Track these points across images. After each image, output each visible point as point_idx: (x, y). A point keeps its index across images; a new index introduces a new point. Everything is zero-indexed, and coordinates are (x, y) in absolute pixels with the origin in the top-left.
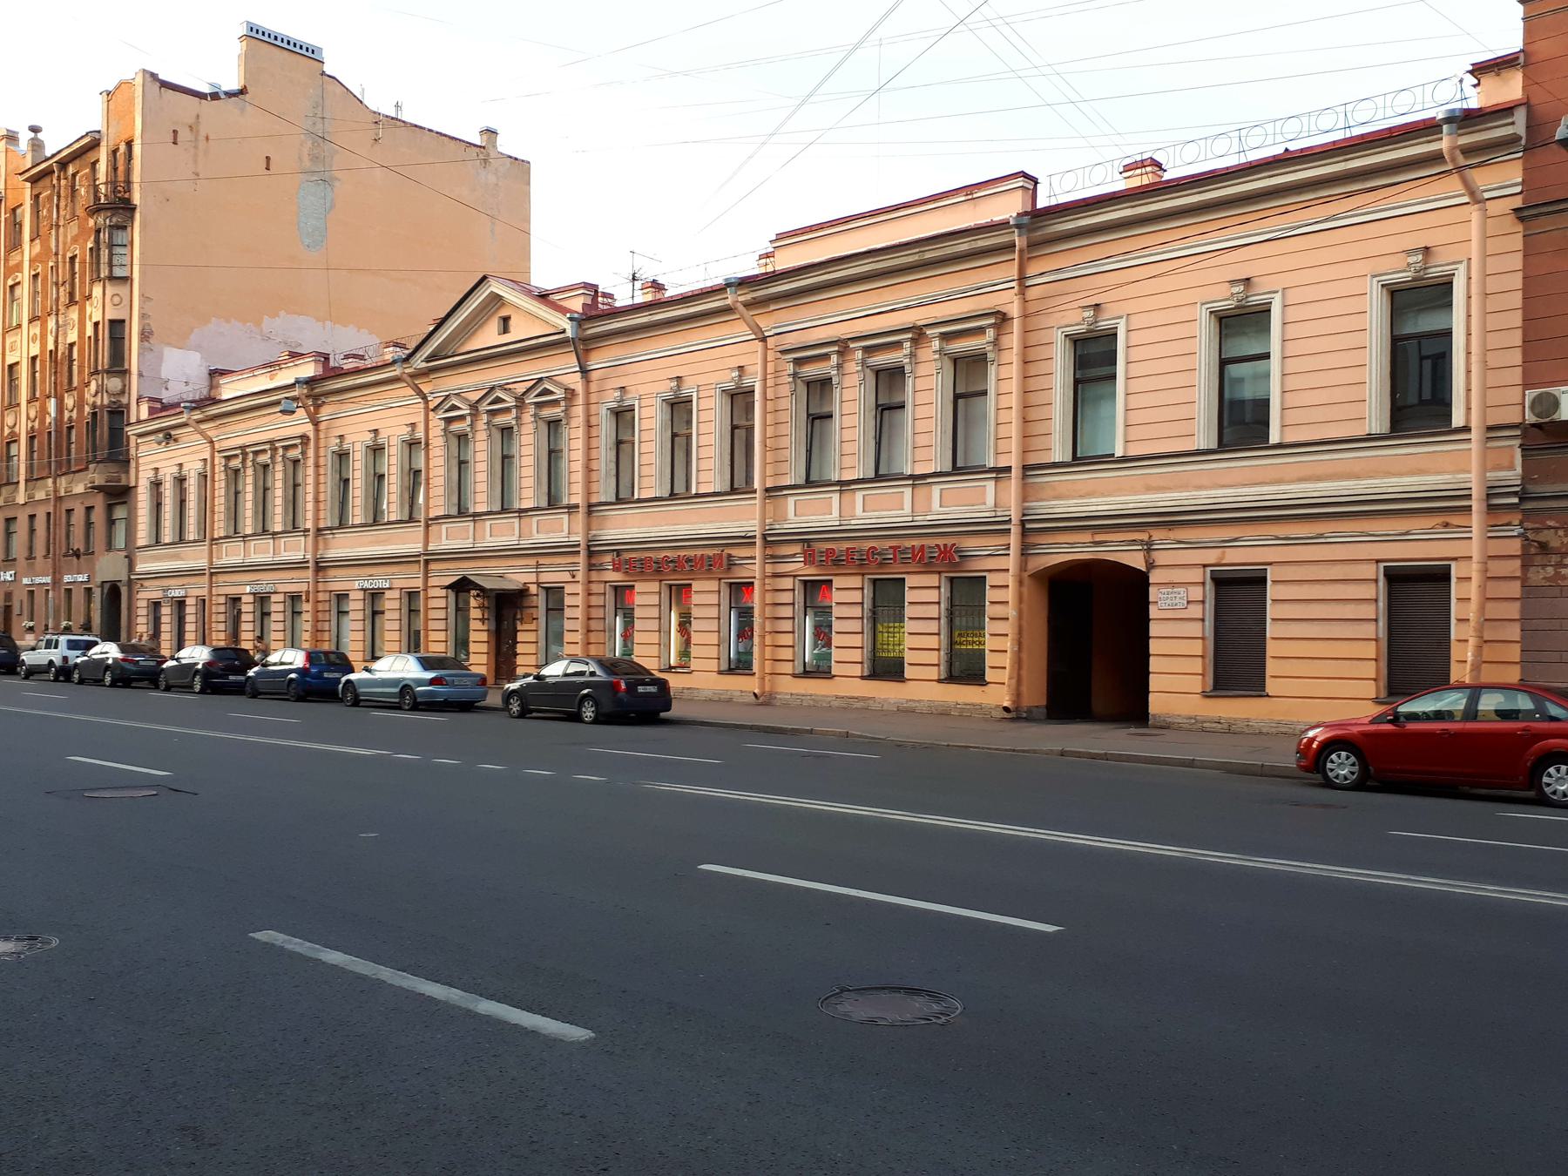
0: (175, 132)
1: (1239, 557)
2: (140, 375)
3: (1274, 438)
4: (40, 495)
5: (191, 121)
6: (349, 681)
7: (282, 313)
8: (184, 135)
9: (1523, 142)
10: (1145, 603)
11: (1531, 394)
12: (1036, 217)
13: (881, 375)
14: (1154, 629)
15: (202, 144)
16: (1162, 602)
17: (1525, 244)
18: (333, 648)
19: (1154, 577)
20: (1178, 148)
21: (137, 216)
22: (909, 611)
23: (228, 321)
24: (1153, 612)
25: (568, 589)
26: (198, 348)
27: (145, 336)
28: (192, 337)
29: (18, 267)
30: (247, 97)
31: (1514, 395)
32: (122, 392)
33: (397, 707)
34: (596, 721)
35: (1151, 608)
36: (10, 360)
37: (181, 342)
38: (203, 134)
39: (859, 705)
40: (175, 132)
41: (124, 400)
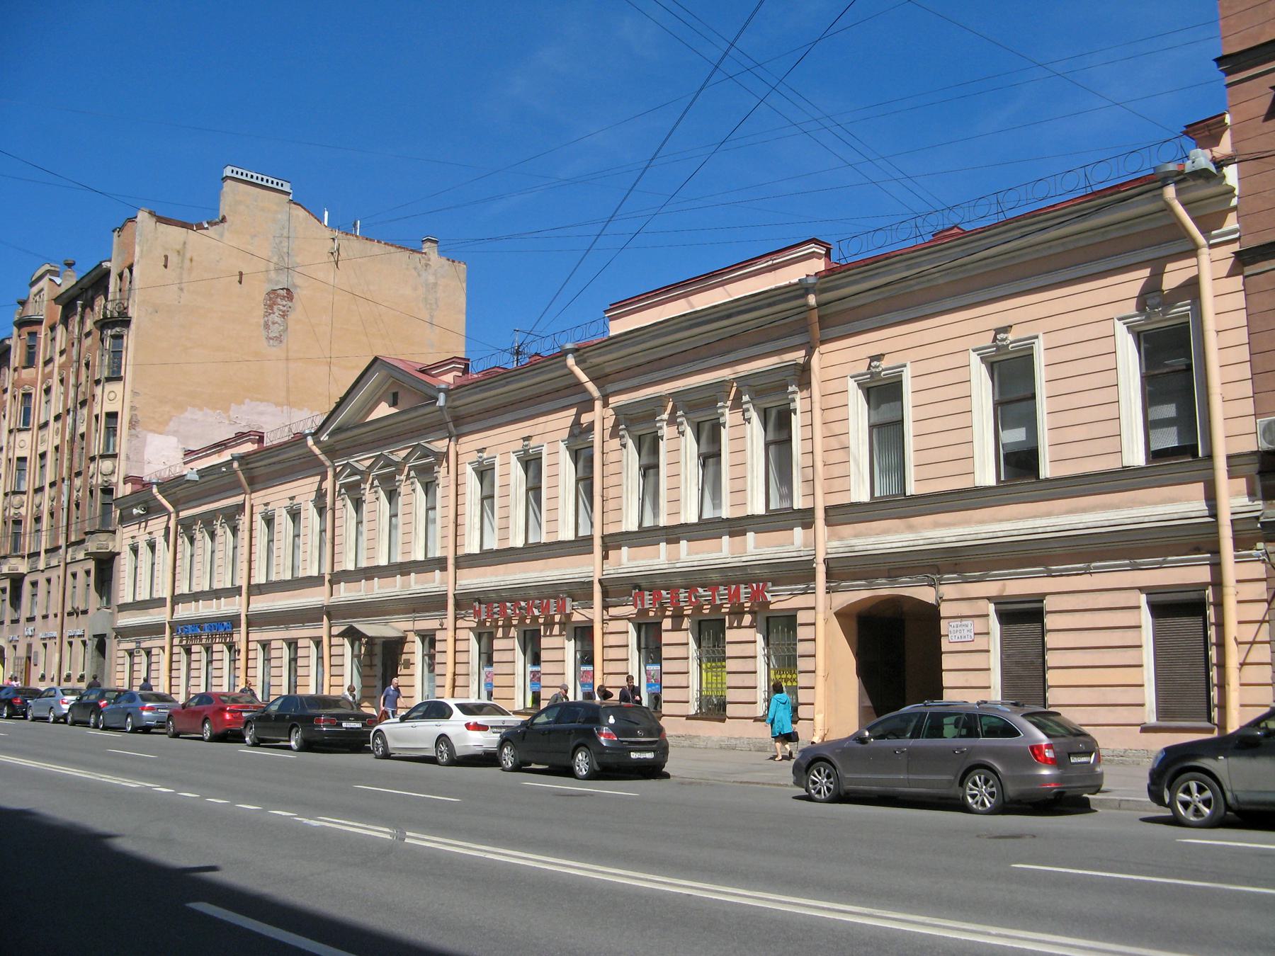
0: (166, 257)
1: (1020, 586)
2: (128, 458)
3: (1046, 471)
4: (54, 563)
5: (178, 247)
6: (379, 730)
7: (247, 401)
8: (173, 259)
9: (1236, 192)
10: (937, 636)
11: (1263, 421)
12: (265, 452)
13: (996, 366)
14: (947, 662)
15: (187, 262)
16: (953, 634)
17: (1244, 284)
18: (126, 687)
19: (945, 610)
20: (1059, 177)
21: (133, 326)
22: (730, 650)
23: (201, 409)
24: (945, 646)
25: (439, 635)
26: (175, 433)
27: (133, 424)
28: (171, 424)
29: (50, 375)
30: (226, 225)
31: (1249, 424)
32: (113, 472)
33: (432, 760)
34: (593, 776)
35: (944, 641)
36: (41, 450)
37: (161, 427)
38: (188, 256)
39: (686, 743)
40: (166, 257)
41: (114, 479)
